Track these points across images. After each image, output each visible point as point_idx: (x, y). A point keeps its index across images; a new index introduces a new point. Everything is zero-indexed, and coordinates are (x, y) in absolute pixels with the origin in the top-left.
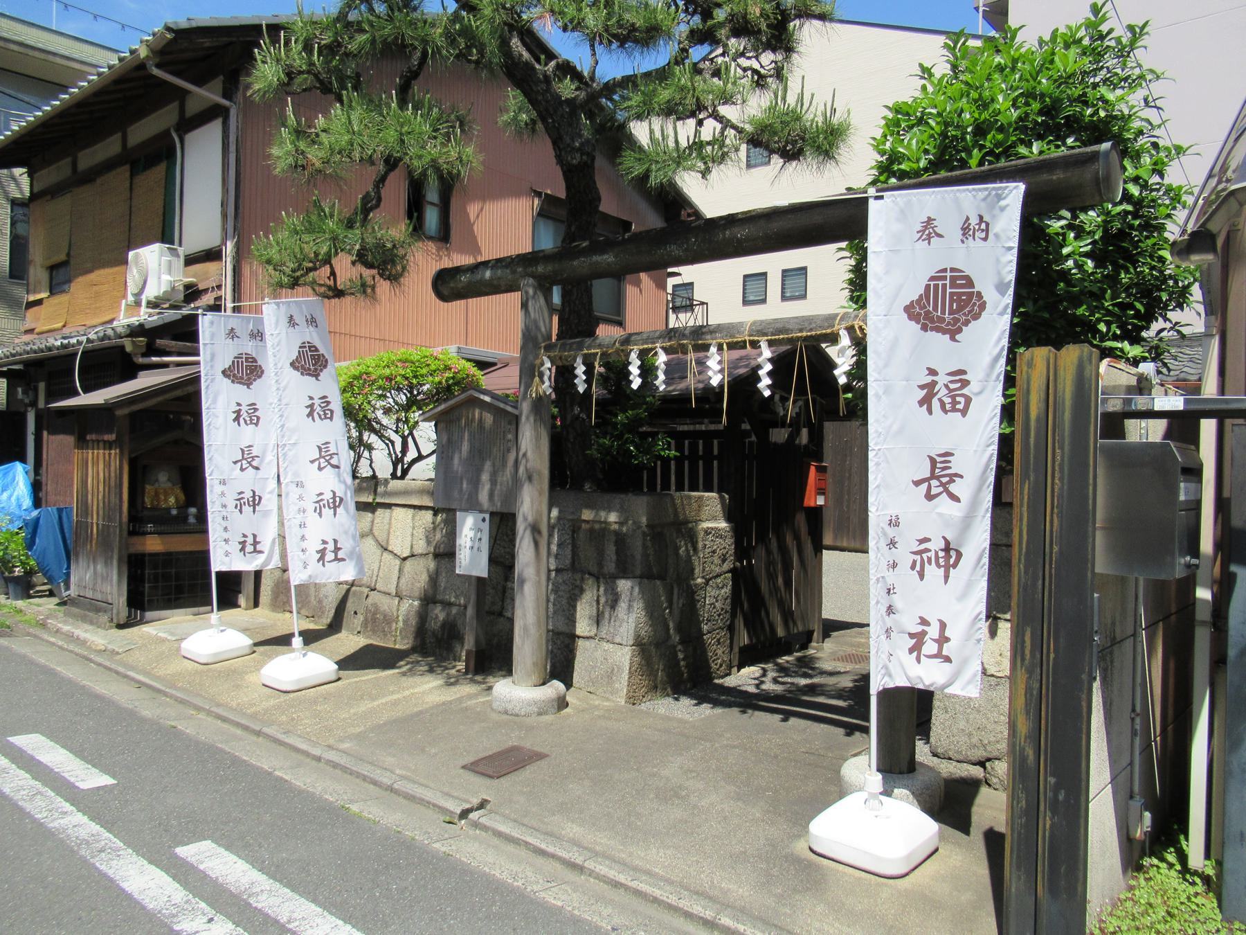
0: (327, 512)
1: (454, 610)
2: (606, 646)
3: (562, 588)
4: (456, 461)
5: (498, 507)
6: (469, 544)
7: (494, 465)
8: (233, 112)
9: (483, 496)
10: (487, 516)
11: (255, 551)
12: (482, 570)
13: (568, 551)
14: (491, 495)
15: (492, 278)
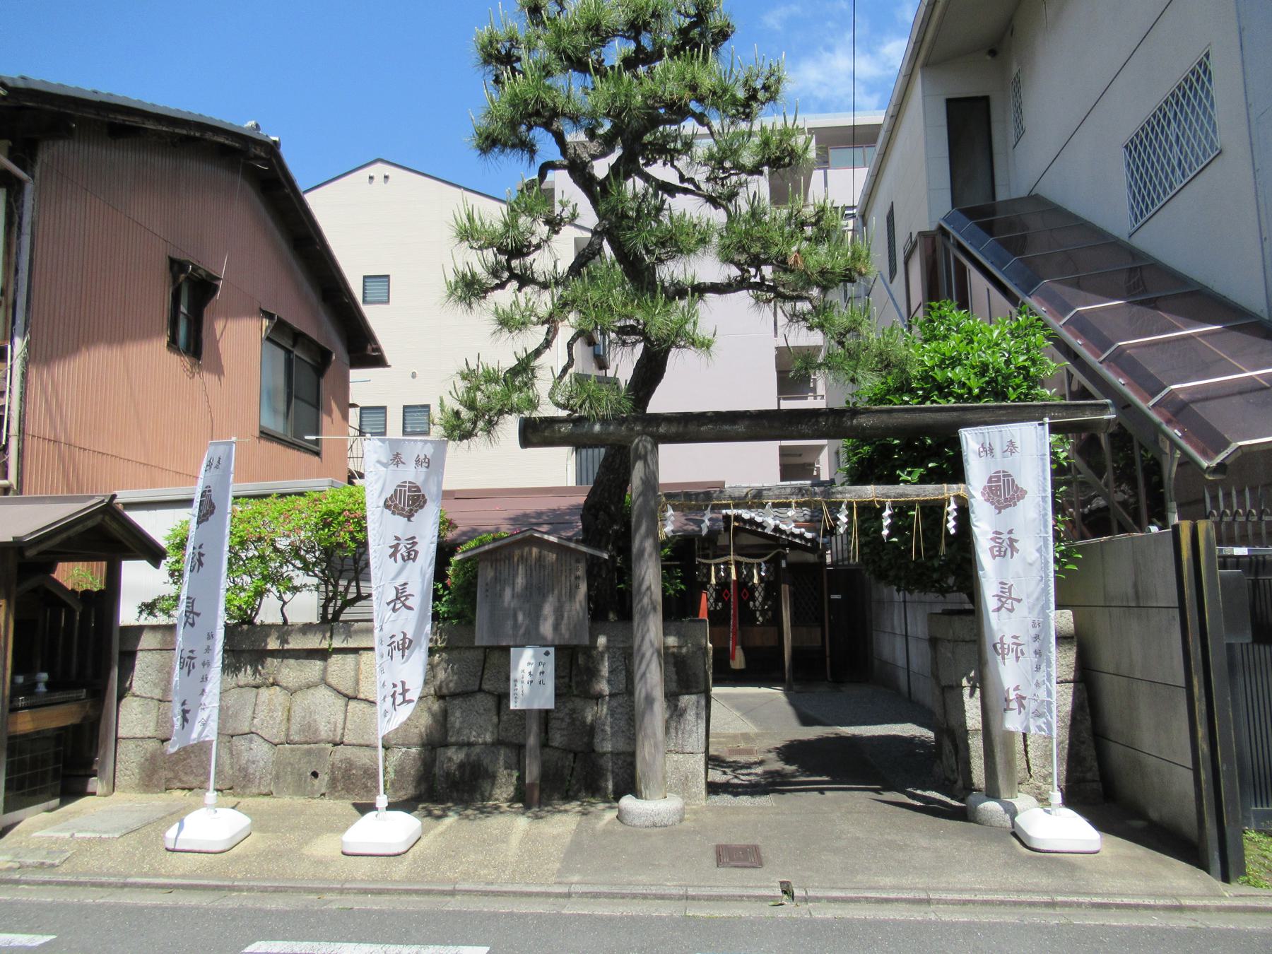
0: (397, 654)
1: (477, 750)
2: (675, 757)
3: (619, 710)
4: (508, 593)
5: (566, 636)
6: (527, 678)
7: (559, 601)
8: (29, 188)
9: (547, 628)
10: (552, 650)
11: (404, 701)
12: (546, 700)
13: (622, 676)
14: (556, 627)
15: (601, 433)
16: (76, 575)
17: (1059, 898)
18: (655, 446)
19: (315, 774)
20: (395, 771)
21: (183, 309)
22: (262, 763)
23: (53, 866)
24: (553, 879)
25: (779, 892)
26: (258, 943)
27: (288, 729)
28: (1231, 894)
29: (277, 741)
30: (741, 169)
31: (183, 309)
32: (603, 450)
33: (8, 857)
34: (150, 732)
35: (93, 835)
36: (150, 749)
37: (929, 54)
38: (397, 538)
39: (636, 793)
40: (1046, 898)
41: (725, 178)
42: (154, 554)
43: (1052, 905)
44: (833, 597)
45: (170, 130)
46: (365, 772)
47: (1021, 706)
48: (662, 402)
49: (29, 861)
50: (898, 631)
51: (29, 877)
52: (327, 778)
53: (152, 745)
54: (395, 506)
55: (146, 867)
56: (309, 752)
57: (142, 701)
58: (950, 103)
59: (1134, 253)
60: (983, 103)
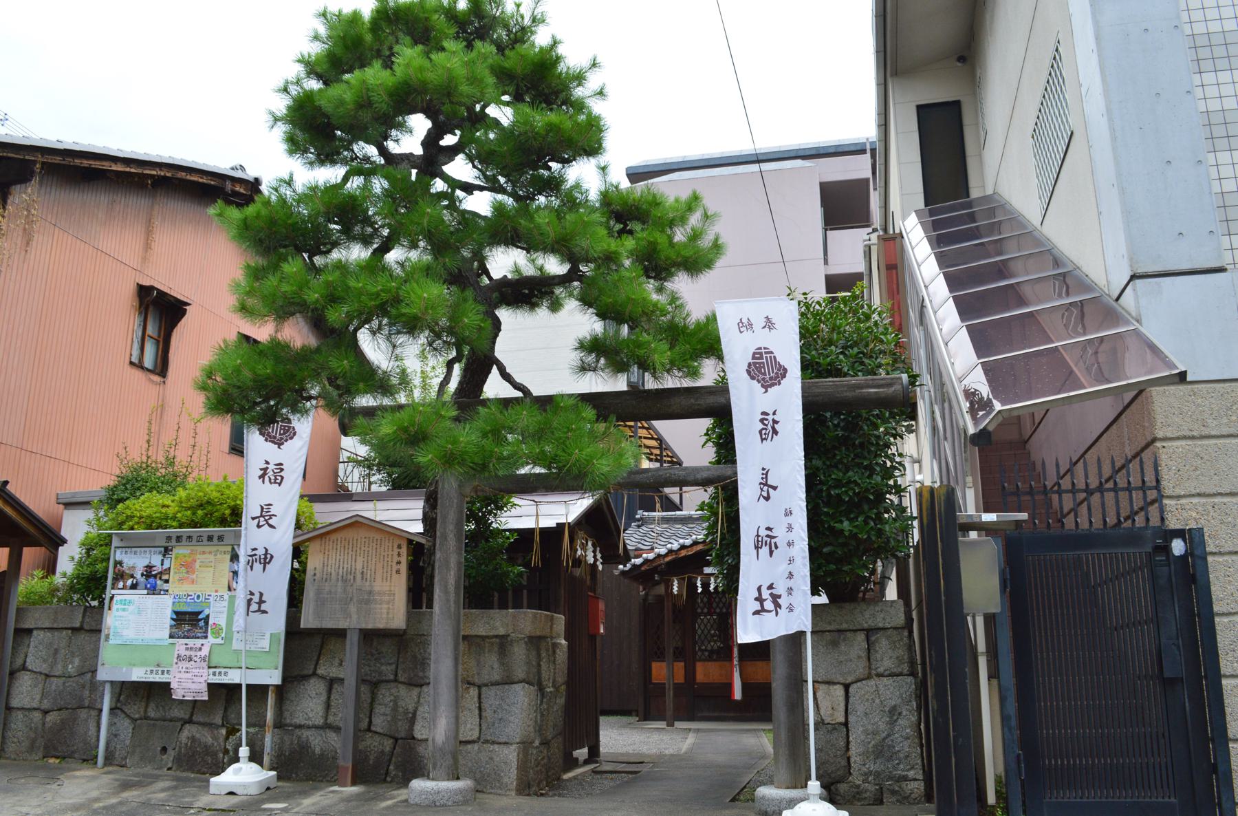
18: (485, 403)
19: (164, 750)
37: (893, 61)
38: (267, 463)
45: (139, 171)
47: (777, 606)
57: (33, 676)
58: (920, 108)
60: (954, 108)
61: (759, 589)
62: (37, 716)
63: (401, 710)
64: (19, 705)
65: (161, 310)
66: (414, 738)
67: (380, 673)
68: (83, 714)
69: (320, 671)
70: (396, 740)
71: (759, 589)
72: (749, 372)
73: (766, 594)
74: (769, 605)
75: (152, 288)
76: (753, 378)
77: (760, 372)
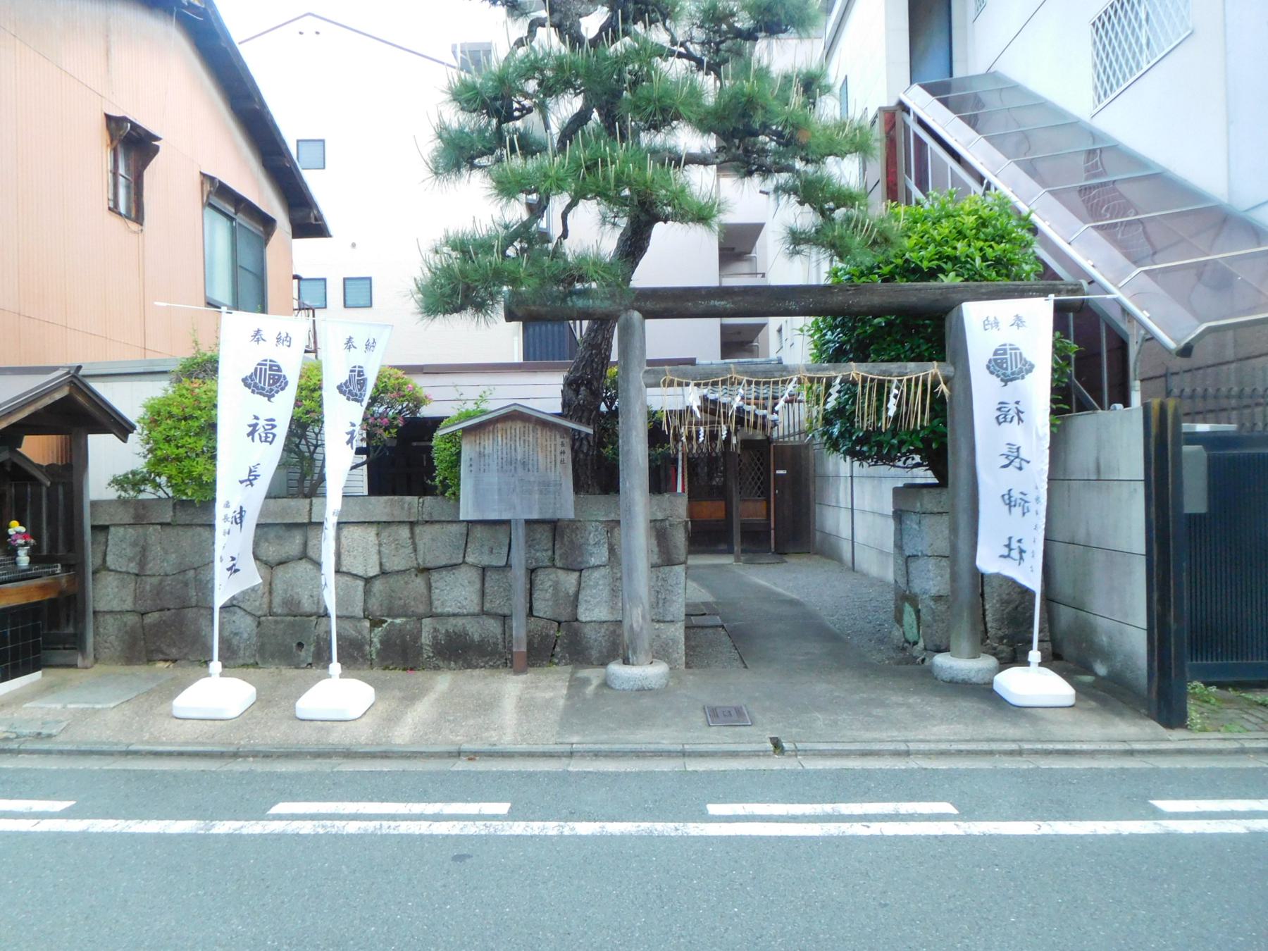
16: (38, 449)
17: (1026, 746)
20: (381, 642)
21: (122, 171)
22: (245, 636)
23: (50, 736)
24: (553, 740)
25: (770, 746)
26: (281, 804)
27: (271, 602)
28: (1176, 738)
29: (260, 613)
30: (739, 34)
31: (122, 171)
32: (585, 323)
33: (4, 729)
34: (128, 605)
35: (86, 706)
36: (129, 623)
39: (626, 662)
40: (1014, 746)
41: (722, 42)
42: (122, 428)
43: (1020, 753)
44: (779, 472)
46: (351, 644)
48: (647, 275)
49: (26, 731)
50: (842, 505)
51: (29, 746)
52: (312, 648)
53: (132, 619)
54: (255, 385)
55: (147, 736)
56: (292, 625)
59: (1094, 135)
61: (1010, 538)
62: (132, 619)
63: (562, 594)
64: (106, 609)
65: (133, 144)
66: (577, 620)
67: (537, 560)
68: (190, 613)
69: (469, 559)
70: (559, 623)
71: (1010, 538)
72: (988, 367)
73: (1014, 545)
74: (1015, 554)
75: (124, 119)
76: (992, 373)
77: (1001, 367)
